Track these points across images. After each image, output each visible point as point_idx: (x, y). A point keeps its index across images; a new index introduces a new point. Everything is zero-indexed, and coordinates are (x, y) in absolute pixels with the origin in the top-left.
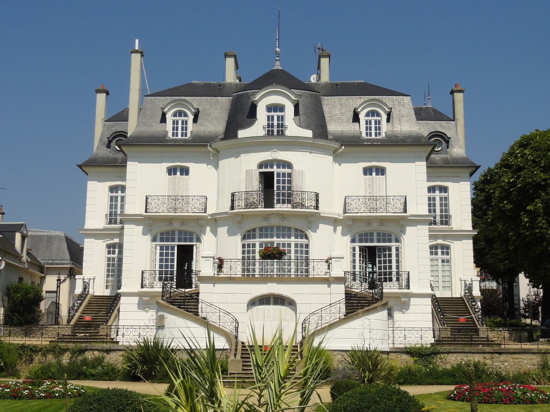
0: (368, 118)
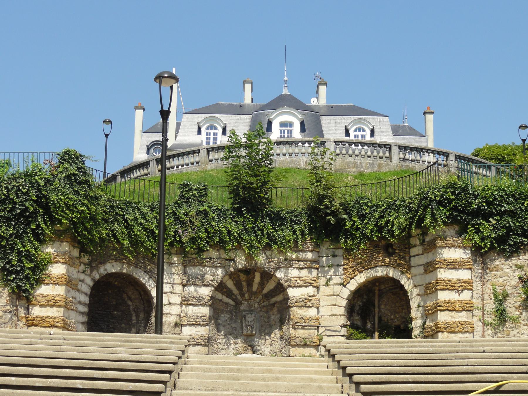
0: (356, 133)
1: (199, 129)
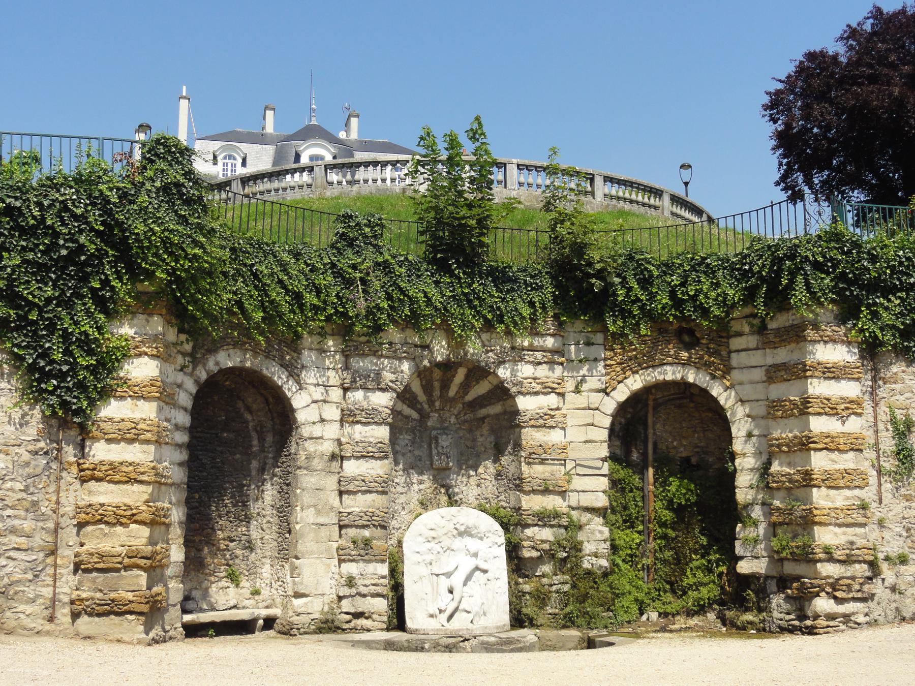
1: (215, 157)
